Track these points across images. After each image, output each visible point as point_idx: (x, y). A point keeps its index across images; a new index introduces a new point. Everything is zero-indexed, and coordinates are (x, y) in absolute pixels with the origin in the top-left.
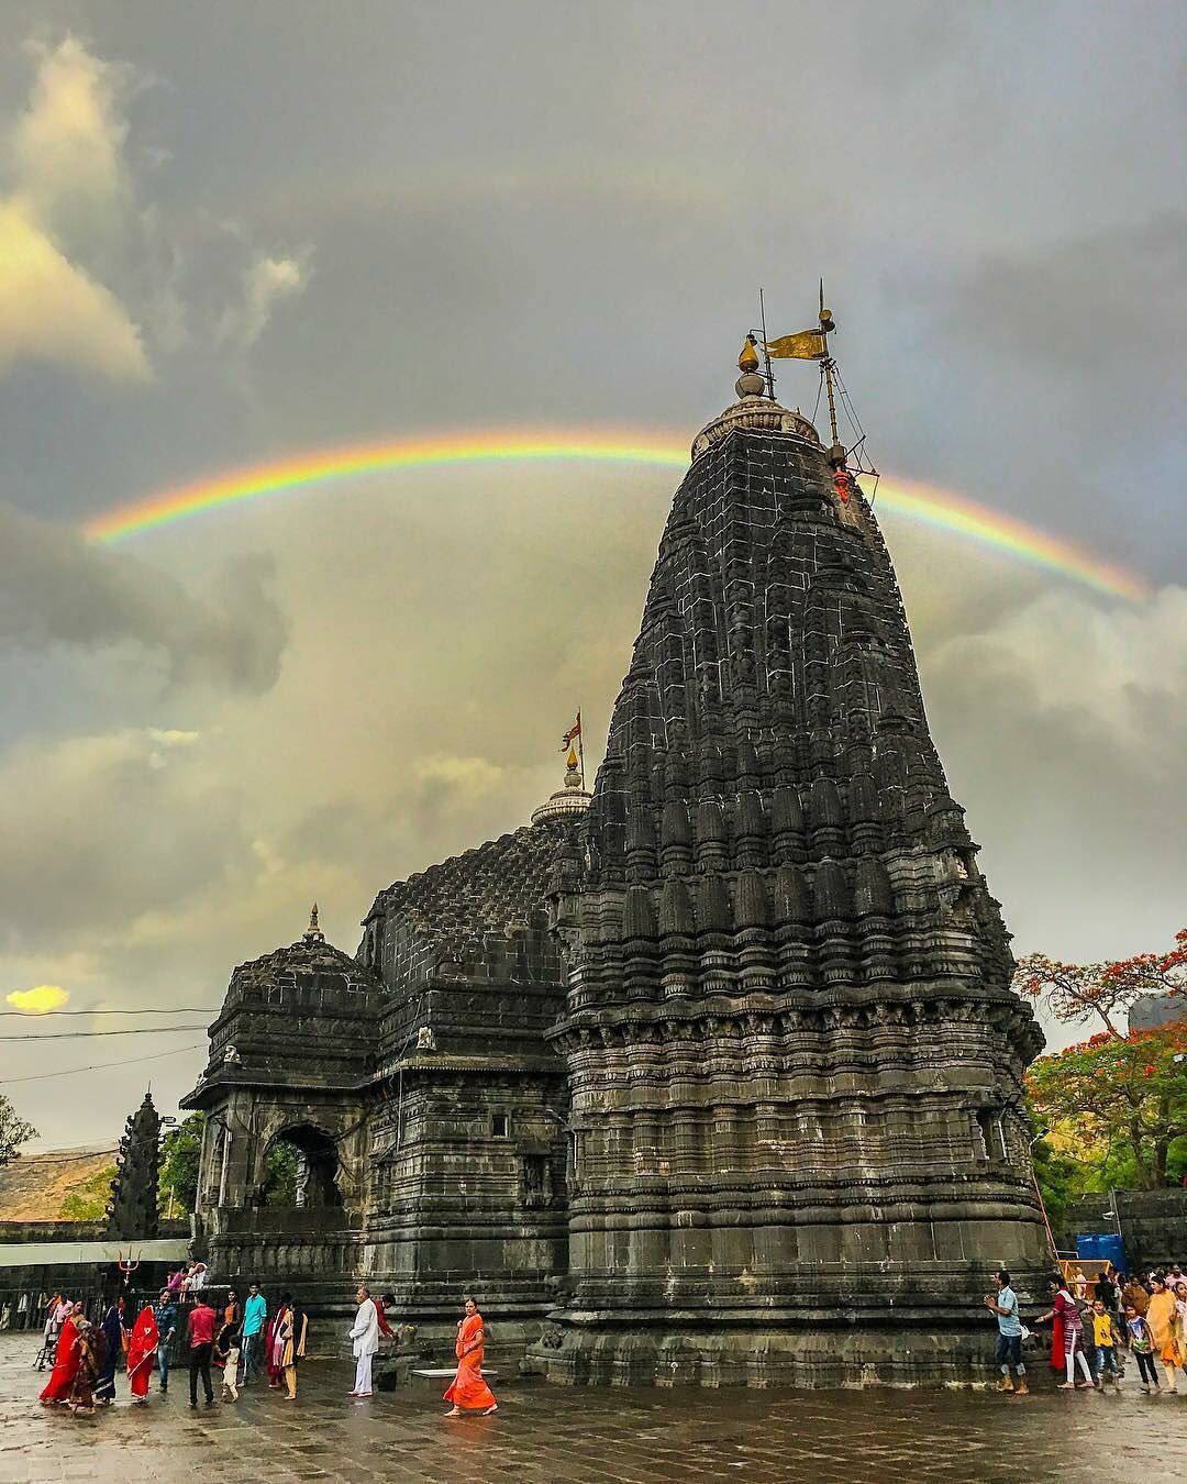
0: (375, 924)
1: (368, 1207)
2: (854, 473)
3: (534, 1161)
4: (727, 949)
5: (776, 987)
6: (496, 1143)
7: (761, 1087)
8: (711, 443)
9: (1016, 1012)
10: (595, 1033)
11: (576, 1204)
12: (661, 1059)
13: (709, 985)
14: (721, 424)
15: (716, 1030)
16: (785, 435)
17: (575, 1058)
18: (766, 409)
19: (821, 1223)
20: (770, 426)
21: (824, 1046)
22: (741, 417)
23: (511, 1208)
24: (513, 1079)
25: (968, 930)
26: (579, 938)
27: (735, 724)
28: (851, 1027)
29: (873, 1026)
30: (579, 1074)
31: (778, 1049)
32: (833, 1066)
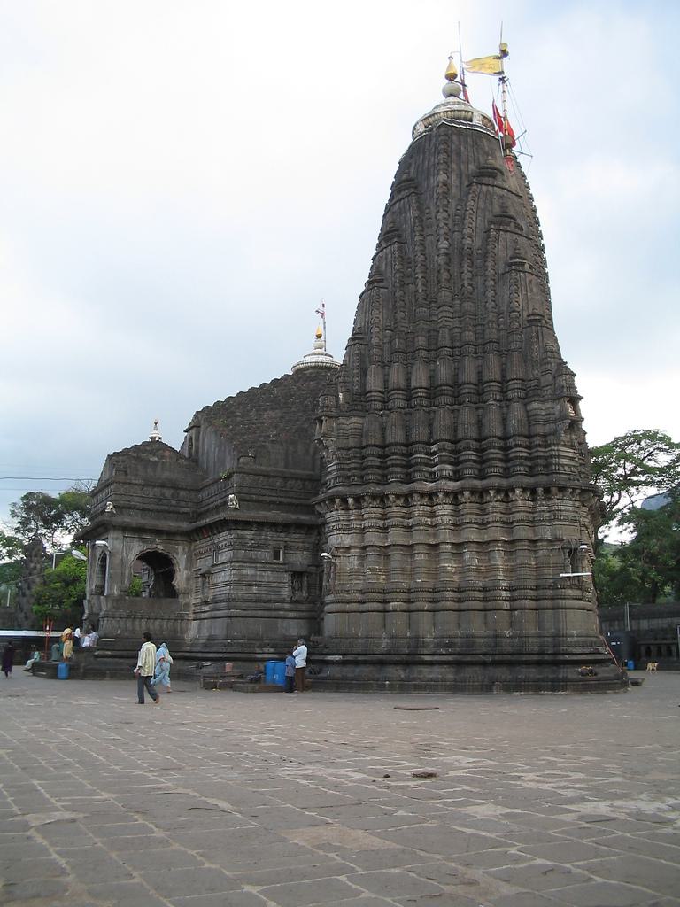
0: (194, 431)
1: (193, 599)
2: (517, 154)
3: (297, 575)
4: (427, 454)
5: (456, 477)
6: (275, 564)
7: (446, 535)
8: (426, 127)
9: (595, 496)
10: (344, 501)
11: (329, 598)
12: (409, 516)
13: (417, 474)
14: (434, 115)
15: (495, 497)
16: (475, 126)
17: (330, 516)
18: (463, 107)
19: (342, 612)
20: (465, 119)
21: (483, 512)
22: (447, 112)
23: (283, 601)
24: (286, 527)
25: (572, 447)
26: (332, 443)
27: (437, 315)
28: (499, 501)
29: (512, 501)
30: (333, 524)
31: (456, 514)
32: (488, 523)
